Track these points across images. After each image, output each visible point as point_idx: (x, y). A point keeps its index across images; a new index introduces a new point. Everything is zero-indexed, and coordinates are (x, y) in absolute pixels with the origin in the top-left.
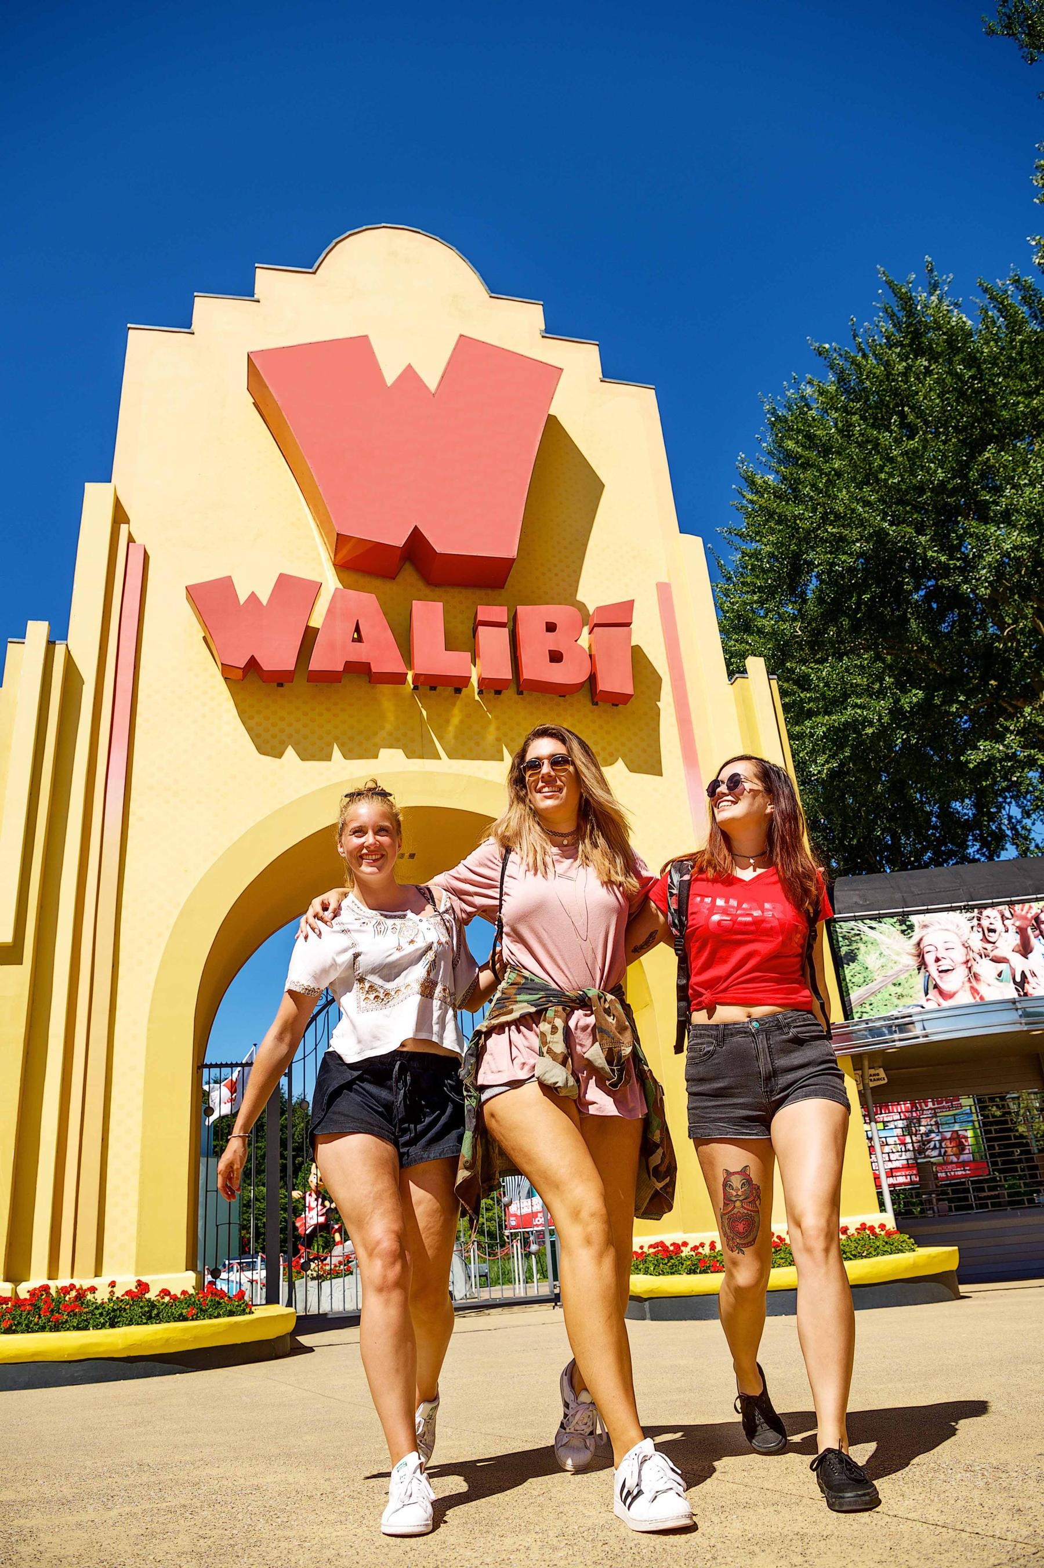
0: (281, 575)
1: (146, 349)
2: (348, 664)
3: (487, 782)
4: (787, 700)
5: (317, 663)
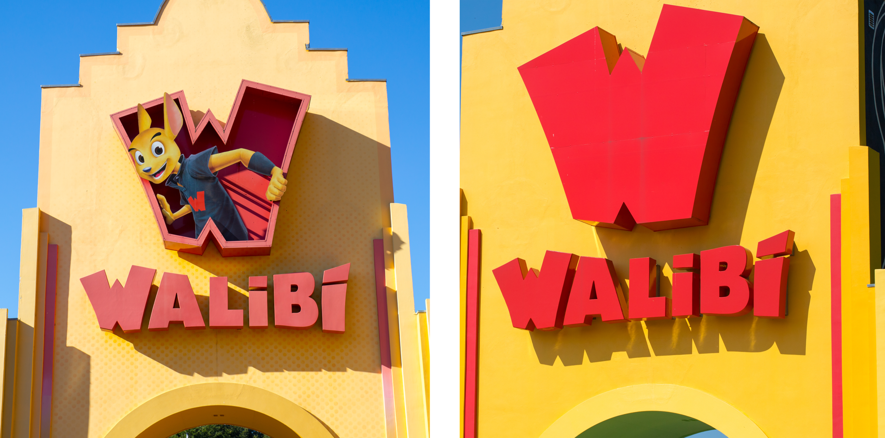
0: (133, 267)
1: (52, 100)
2: (171, 323)
3: (254, 388)
4: (753, 343)
5: (153, 324)
